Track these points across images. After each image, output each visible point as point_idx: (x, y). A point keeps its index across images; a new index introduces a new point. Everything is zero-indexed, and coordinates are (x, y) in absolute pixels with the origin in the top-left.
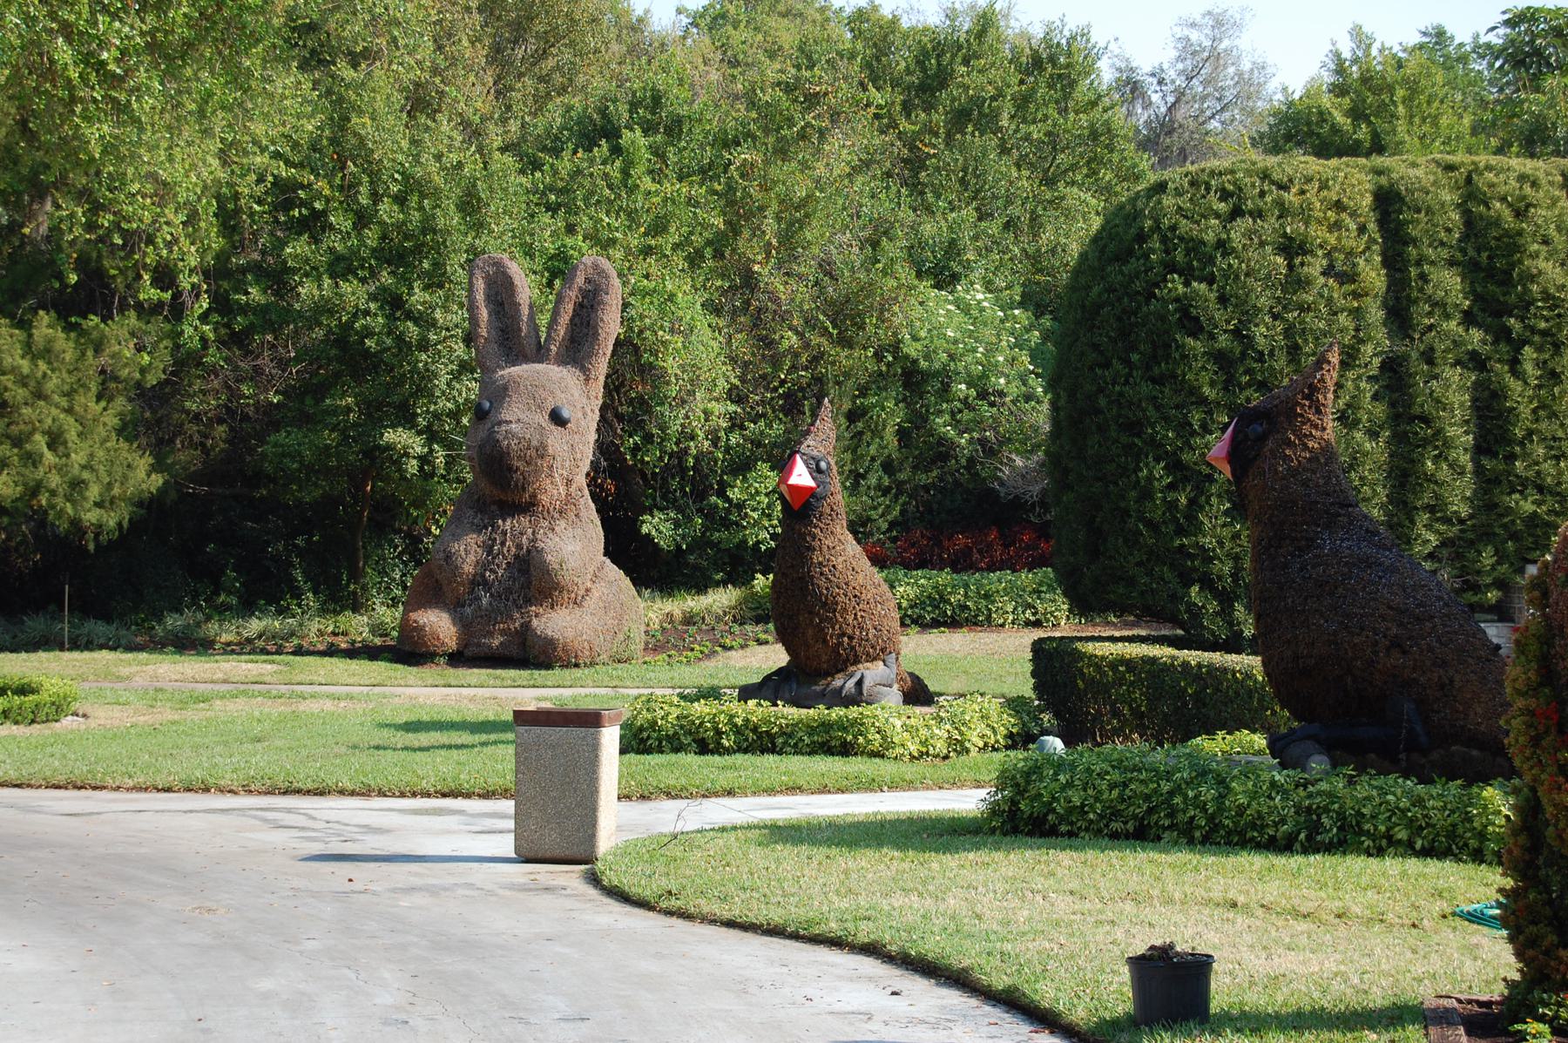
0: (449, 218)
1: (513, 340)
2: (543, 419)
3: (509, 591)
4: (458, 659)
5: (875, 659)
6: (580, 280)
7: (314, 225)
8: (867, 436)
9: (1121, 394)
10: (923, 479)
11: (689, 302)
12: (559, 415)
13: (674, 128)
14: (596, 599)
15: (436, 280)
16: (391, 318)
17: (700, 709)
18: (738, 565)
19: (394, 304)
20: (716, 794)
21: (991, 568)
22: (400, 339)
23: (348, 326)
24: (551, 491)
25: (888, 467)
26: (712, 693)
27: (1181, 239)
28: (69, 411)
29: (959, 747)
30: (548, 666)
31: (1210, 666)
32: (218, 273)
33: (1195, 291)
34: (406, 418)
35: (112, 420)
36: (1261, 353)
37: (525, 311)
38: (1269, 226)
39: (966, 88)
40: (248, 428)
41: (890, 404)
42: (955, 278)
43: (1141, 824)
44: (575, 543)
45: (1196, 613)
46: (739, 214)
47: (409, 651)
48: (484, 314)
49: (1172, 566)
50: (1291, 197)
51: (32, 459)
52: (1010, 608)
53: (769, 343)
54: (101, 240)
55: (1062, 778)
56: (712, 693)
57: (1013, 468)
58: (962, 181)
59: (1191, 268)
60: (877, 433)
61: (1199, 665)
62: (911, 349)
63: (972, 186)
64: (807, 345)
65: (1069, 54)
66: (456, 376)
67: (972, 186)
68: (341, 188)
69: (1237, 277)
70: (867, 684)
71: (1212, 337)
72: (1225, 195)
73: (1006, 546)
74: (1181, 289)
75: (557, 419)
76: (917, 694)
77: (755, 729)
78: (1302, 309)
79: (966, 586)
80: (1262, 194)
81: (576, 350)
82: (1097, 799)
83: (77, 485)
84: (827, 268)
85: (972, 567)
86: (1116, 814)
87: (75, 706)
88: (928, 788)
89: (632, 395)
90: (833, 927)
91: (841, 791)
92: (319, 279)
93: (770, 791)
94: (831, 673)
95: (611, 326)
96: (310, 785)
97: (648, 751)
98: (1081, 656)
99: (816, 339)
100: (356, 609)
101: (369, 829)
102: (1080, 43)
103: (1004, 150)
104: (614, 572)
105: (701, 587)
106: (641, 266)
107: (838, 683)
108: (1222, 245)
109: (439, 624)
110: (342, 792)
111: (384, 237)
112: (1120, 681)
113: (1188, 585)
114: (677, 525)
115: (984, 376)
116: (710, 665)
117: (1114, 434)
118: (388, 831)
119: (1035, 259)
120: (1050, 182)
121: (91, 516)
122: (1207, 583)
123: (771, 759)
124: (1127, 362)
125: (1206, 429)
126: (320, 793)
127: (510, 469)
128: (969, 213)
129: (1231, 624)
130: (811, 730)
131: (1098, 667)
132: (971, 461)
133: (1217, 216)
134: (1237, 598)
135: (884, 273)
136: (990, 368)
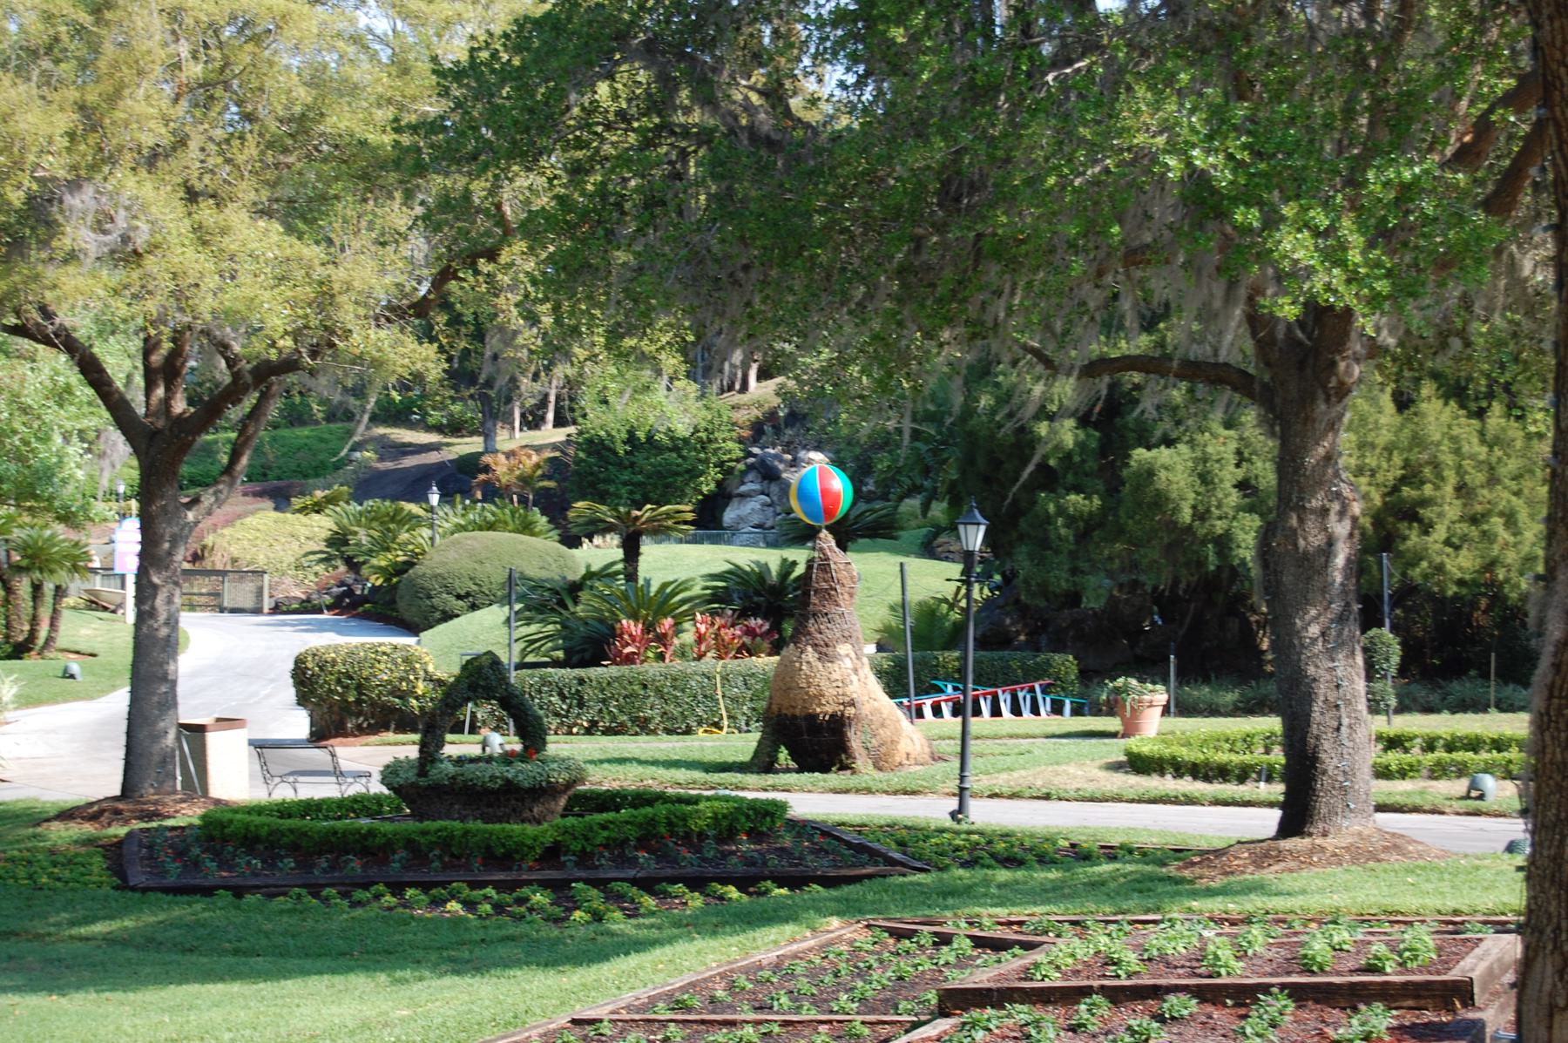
28: (1517, 494)
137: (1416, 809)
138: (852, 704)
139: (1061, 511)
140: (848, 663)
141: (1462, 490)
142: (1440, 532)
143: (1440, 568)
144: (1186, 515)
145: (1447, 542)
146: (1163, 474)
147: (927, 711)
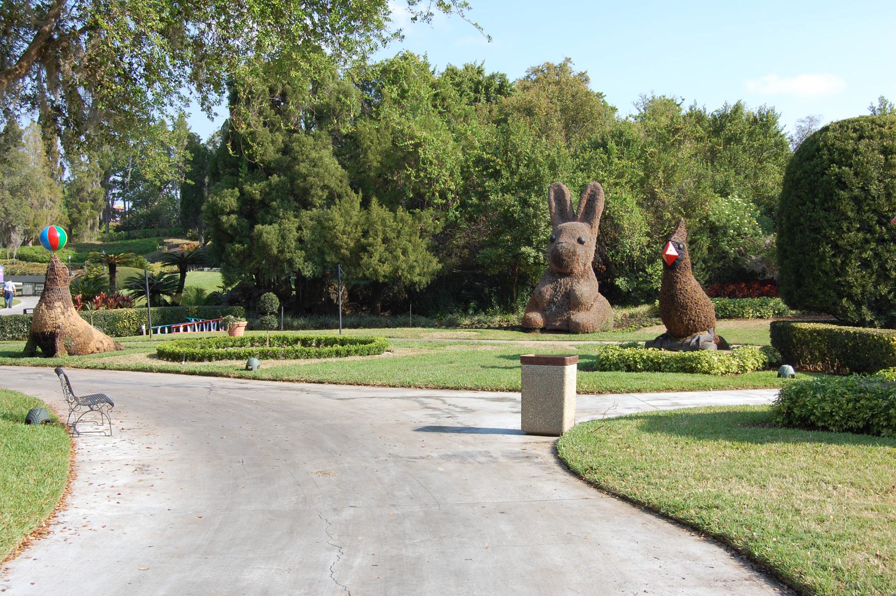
0: (545, 171)
1: (563, 213)
2: (575, 242)
3: (562, 305)
4: (544, 330)
5: (705, 330)
6: (589, 191)
7: (496, 175)
8: (697, 250)
9: (811, 216)
10: (716, 265)
11: (631, 202)
12: (582, 241)
13: (628, 143)
14: (594, 306)
15: (539, 193)
16: (523, 207)
17: (628, 351)
18: (649, 297)
19: (524, 203)
20: (633, 392)
21: (744, 297)
22: (527, 215)
23: (508, 210)
24: (578, 268)
25: (704, 261)
26: (634, 345)
27: (837, 149)
28: (410, 241)
29: (743, 369)
30: (577, 333)
31: (860, 333)
32: (465, 193)
33: (844, 171)
34: (529, 243)
35: (425, 246)
36: (874, 197)
37: (569, 203)
38: (876, 143)
39: (730, 130)
40: (474, 248)
41: (705, 238)
42: (728, 194)
43: (868, 423)
44: (587, 287)
45: (845, 310)
46: (649, 170)
47: (526, 327)
48: (554, 204)
49: (835, 290)
50: (885, 130)
51: (396, 258)
52: (751, 311)
53: (660, 218)
54: (420, 182)
55: (818, 395)
56: (634, 345)
57: (752, 260)
58: (730, 161)
59: (842, 161)
60: (700, 249)
61: (855, 333)
62: (712, 218)
63: (733, 162)
64: (674, 218)
65: (767, 117)
66: (547, 227)
67: (733, 162)
68: (505, 162)
69: (862, 164)
70: (701, 341)
71: (852, 190)
72: (855, 131)
73: (749, 289)
74: (837, 170)
75: (580, 241)
76: (722, 345)
77: (652, 361)
78: (892, 178)
79: (734, 303)
80: (872, 129)
81: (588, 216)
82: (840, 408)
83: (412, 268)
84: (682, 191)
85: (736, 297)
86: (851, 417)
87: (386, 348)
88: (731, 389)
89: (610, 235)
90: (691, 513)
91: (691, 390)
92: (498, 193)
93: (658, 390)
94: (685, 336)
95: (600, 207)
96: (453, 385)
97: (605, 370)
98: (795, 329)
99: (677, 215)
100: (513, 313)
101: (467, 410)
102: (771, 113)
103: (744, 151)
104: (602, 298)
105: (636, 305)
106: (613, 190)
107: (688, 340)
108: (856, 151)
109: (537, 317)
110: (466, 389)
111: (521, 179)
112: (815, 339)
113: (841, 298)
114: (628, 282)
115: (739, 228)
116: (638, 332)
117: (808, 233)
118: (474, 411)
119: (756, 188)
120: (761, 162)
121: (416, 279)
122: (850, 297)
123: (658, 375)
124: (813, 202)
125: (849, 230)
126: (457, 389)
127: (563, 260)
128: (732, 172)
129: (860, 315)
130: (677, 361)
131: (803, 334)
132: (735, 258)
133: (852, 139)
134: (864, 304)
135: (703, 191)
136: (741, 225)
137: (221, 375)
138: (59, 327)
139: (233, 251)
140: (59, 310)
141: (385, 240)
142: (377, 256)
143: (375, 271)
144: (275, 251)
145: (380, 261)
146: (265, 235)
147: (181, 329)
